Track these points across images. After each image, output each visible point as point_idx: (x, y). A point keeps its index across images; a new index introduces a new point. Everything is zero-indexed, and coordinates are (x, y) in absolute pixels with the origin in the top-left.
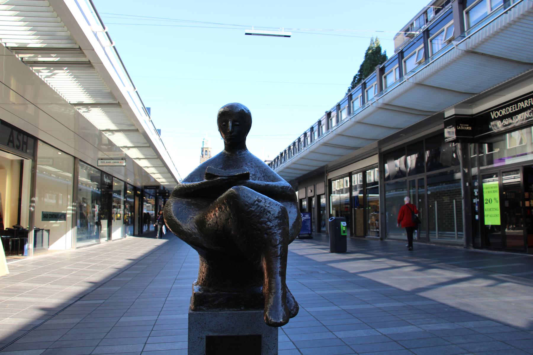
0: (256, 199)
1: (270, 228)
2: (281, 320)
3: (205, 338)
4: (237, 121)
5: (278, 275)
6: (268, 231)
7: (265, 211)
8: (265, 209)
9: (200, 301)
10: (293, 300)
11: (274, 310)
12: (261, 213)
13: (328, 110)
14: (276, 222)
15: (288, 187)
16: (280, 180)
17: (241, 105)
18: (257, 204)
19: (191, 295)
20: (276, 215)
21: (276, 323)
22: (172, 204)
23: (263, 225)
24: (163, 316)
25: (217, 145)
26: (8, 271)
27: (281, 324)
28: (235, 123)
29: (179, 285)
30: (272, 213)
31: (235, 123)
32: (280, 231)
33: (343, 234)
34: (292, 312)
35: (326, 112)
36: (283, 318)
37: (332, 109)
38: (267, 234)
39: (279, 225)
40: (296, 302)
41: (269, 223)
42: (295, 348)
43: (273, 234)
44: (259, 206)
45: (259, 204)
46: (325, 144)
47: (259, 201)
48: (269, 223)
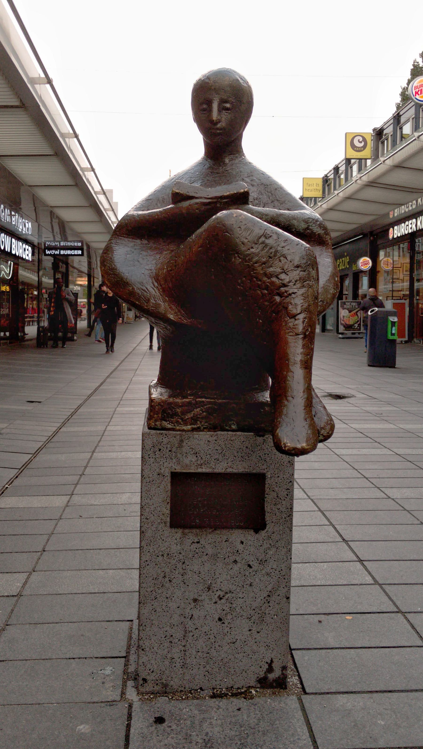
0: (261, 232)
1: (285, 285)
2: (304, 445)
3: (169, 475)
4: (226, 102)
5: (298, 365)
6: (283, 289)
7: (275, 255)
8: (276, 252)
9: (159, 415)
10: (324, 412)
11: (293, 430)
12: (270, 257)
13: (378, 125)
14: (296, 274)
15: (317, 221)
16: (303, 208)
17: (235, 72)
18: (263, 243)
19: (51, 263)
20: (296, 263)
21: (294, 449)
22: (285, 639)
23: (274, 279)
24: (100, 454)
25: (188, 149)
26: (291, 619)
27: (303, 452)
28: (222, 108)
29: (132, 409)
30: (289, 258)
31: (222, 108)
32: (303, 290)
33: (390, 337)
34: (321, 433)
35: (374, 130)
36: (307, 441)
37: (385, 123)
38: (280, 295)
39: (302, 280)
40: (329, 415)
41: (283, 276)
42: (316, 509)
43: (290, 295)
44: (266, 245)
45: (267, 241)
46: (372, 184)
47: (266, 236)
48: (283, 276)
